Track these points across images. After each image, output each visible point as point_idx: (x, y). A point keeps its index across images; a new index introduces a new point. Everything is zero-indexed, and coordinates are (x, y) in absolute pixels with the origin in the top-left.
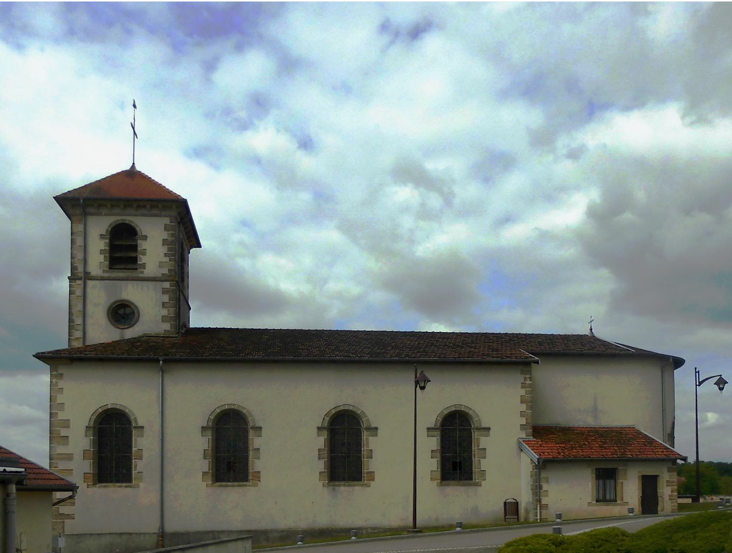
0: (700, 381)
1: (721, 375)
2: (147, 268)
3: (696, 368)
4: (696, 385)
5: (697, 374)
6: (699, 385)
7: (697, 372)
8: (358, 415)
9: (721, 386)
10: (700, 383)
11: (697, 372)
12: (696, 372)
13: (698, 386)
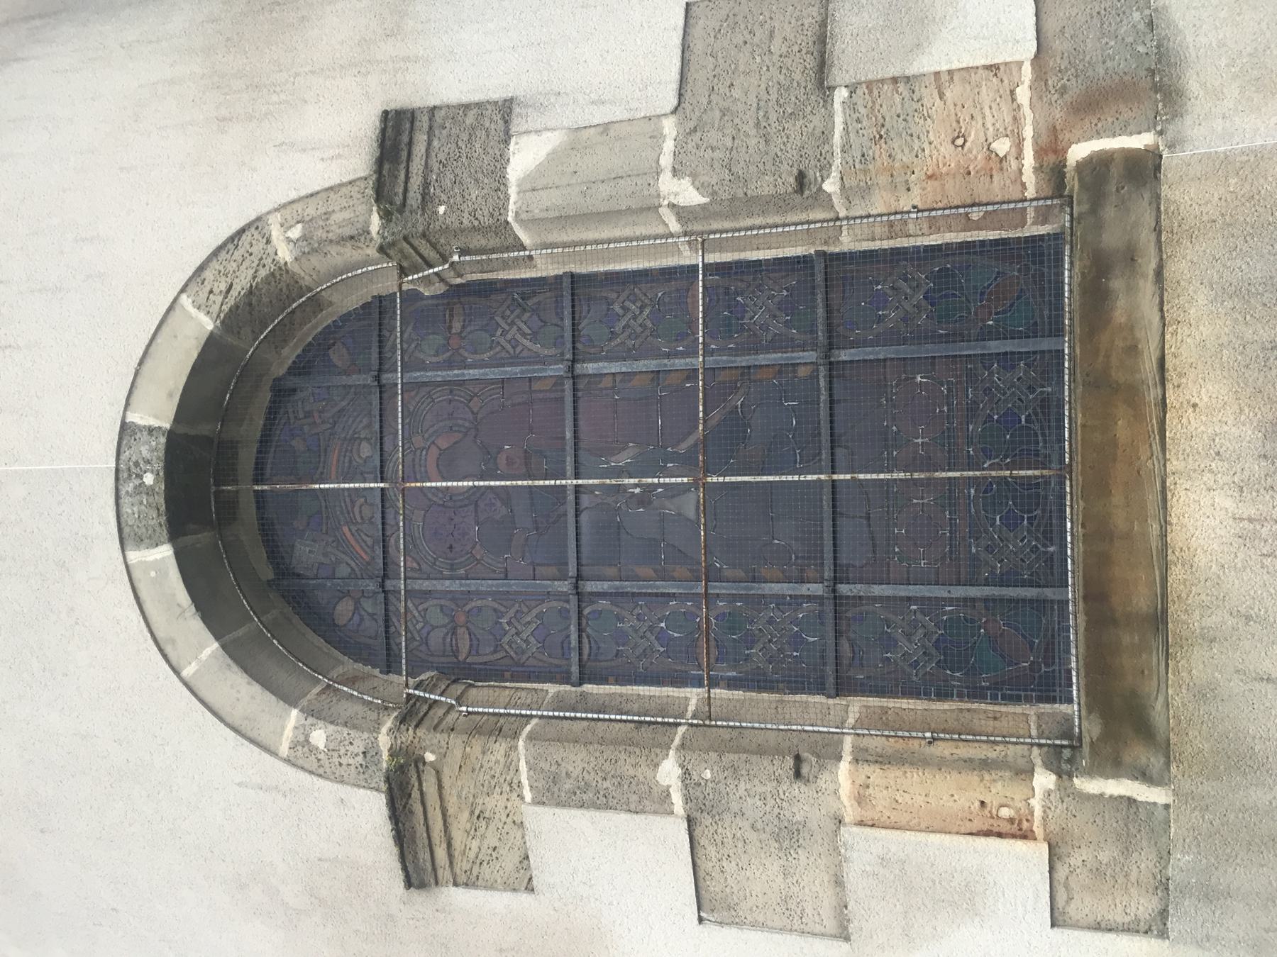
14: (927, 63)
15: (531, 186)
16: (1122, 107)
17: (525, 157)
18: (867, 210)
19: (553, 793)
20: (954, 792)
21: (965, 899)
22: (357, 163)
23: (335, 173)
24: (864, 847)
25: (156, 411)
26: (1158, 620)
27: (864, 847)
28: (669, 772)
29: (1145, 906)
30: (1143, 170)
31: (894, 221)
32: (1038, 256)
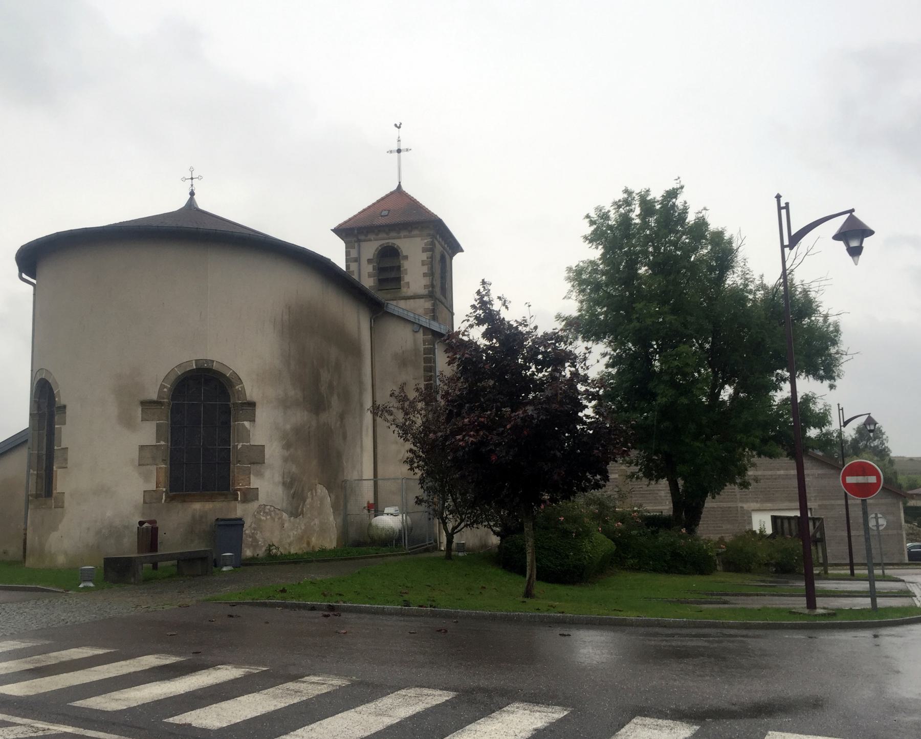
0: (793, 233)
1: (853, 210)
2: (846, 367)
3: (778, 197)
4: (783, 247)
5: (784, 212)
6: (792, 246)
7: (783, 208)
8: (228, 379)
9: (854, 244)
10: (795, 240)
11: (783, 208)
12: (780, 208)
13: (787, 250)
14: (252, 476)
15: (243, 425)
16: (820, 324)
17: (247, 424)
18: (235, 468)
19: (158, 426)
20: (162, 478)
21: (147, 479)
22: (249, 398)
23: (248, 394)
24: (154, 468)
25: (215, 366)
26: (184, 501)
27: (154, 468)
28: (162, 443)
29: (148, 500)
30: (236, 499)
31: (233, 472)
32: (228, 489)
